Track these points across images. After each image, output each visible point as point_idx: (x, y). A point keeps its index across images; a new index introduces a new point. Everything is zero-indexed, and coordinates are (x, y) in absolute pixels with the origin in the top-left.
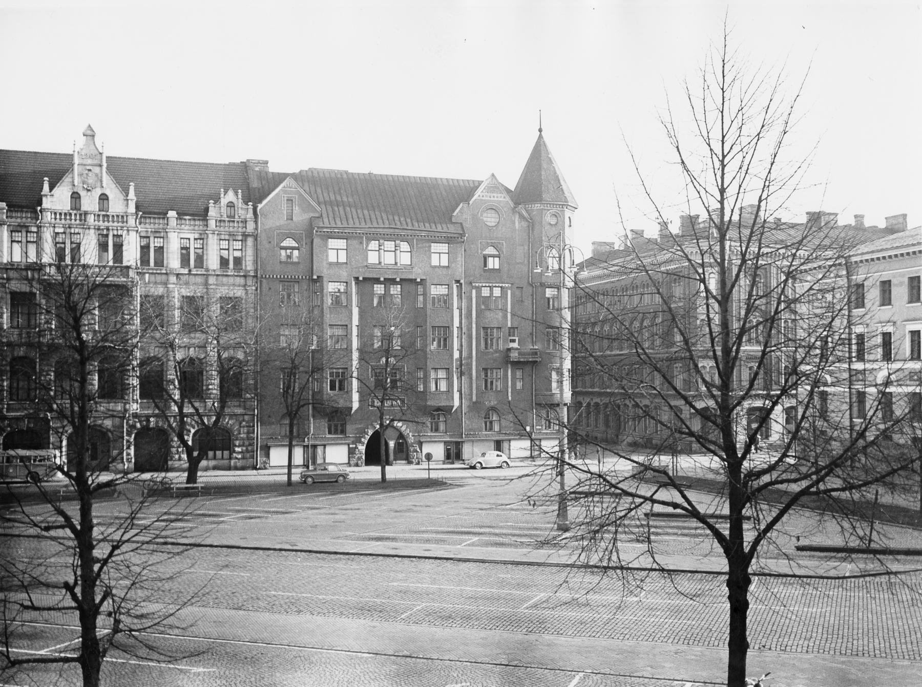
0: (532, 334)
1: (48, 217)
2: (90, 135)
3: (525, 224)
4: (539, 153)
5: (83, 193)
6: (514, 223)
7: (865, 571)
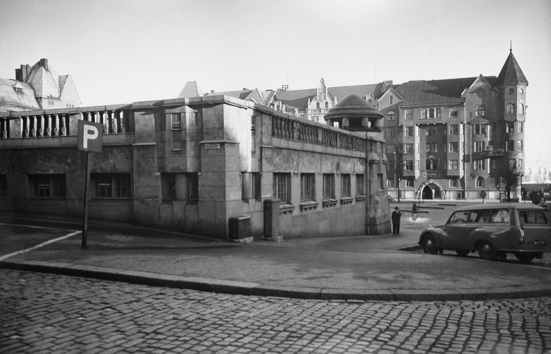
0: (500, 144)
1: (310, 112)
2: (323, 82)
3: (497, 95)
4: (511, 61)
5: (320, 102)
6: (491, 94)
7: (370, 182)
